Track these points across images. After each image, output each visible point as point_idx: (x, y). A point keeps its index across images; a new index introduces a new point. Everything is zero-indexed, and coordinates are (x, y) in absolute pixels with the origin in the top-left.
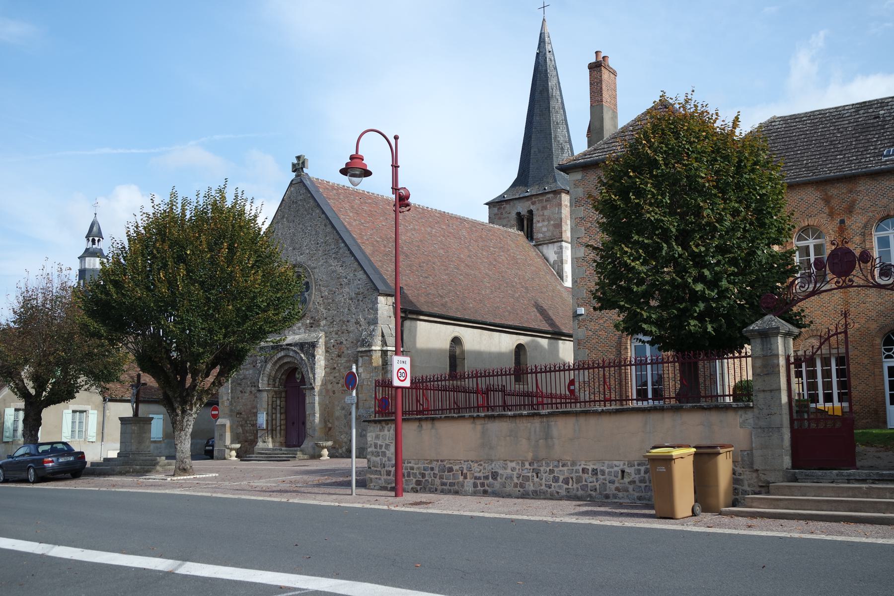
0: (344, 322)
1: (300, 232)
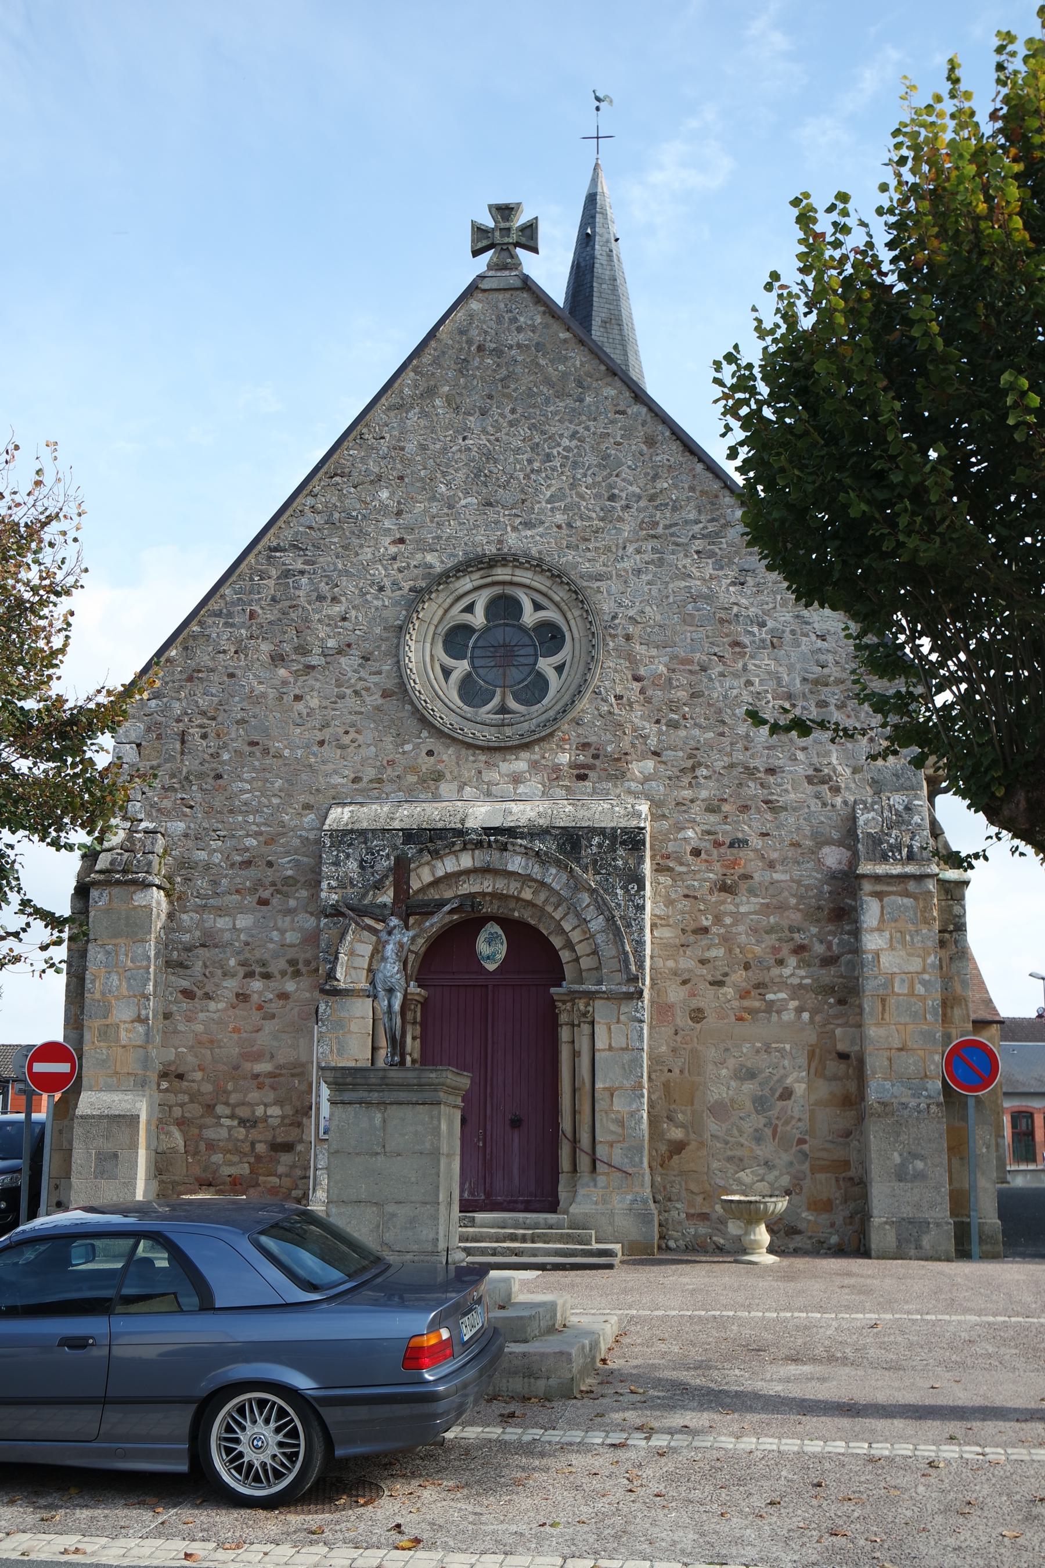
0: (750, 772)
1: (518, 451)
